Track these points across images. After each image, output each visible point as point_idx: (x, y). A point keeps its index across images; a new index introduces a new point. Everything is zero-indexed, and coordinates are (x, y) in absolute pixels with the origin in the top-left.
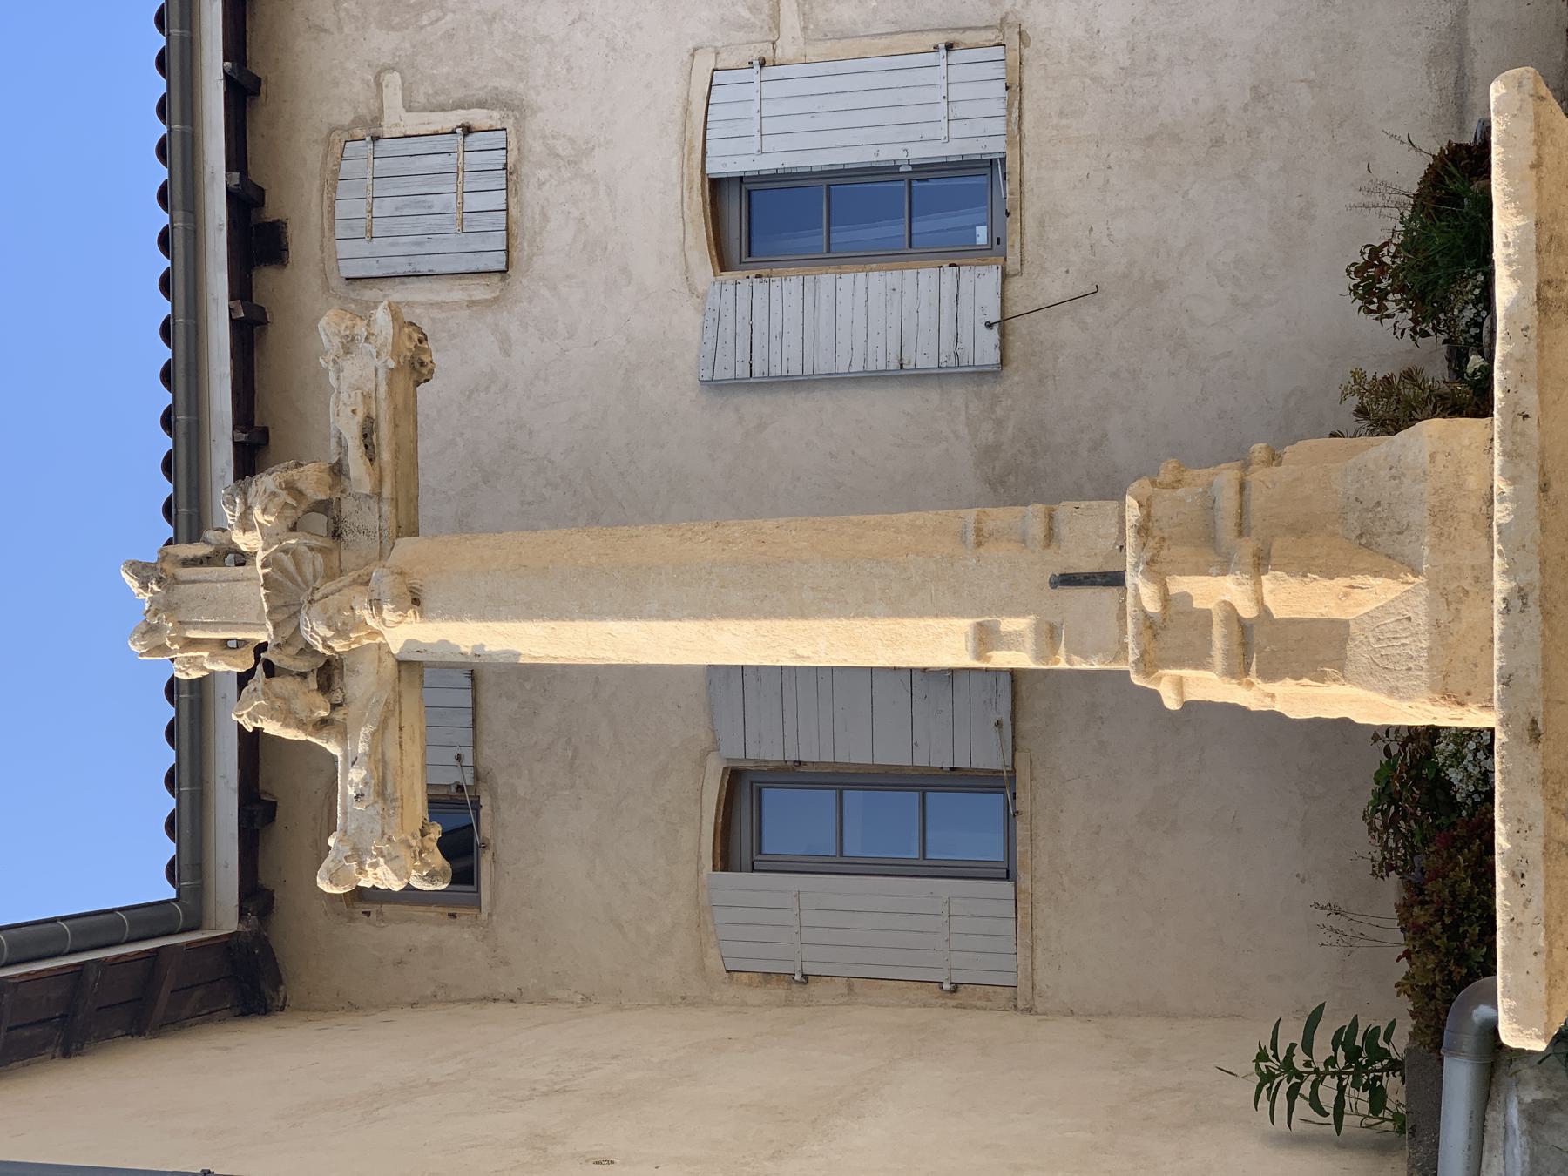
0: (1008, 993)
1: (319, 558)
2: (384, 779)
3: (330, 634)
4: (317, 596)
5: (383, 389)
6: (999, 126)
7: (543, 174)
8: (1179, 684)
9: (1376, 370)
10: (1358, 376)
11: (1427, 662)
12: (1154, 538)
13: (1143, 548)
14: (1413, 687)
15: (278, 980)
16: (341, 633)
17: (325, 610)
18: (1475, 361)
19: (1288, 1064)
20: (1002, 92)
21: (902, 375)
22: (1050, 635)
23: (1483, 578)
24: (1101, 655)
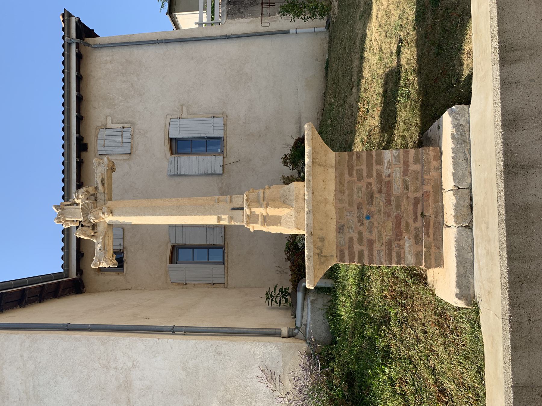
0: (223, 285)
1: (92, 205)
2: (105, 246)
3: (94, 219)
4: (92, 212)
5: (106, 173)
6: (222, 131)
7: (138, 136)
8: (253, 227)
9: (286, 175)
10: (283, 176)
11: (295, 223)
15: (84, 287)
16: (97, 219)
17: (93, 214)
18: (302, 174)
19: (271, 295)
21: (205, 175)
22: (231, 218)
23: (303, 209)
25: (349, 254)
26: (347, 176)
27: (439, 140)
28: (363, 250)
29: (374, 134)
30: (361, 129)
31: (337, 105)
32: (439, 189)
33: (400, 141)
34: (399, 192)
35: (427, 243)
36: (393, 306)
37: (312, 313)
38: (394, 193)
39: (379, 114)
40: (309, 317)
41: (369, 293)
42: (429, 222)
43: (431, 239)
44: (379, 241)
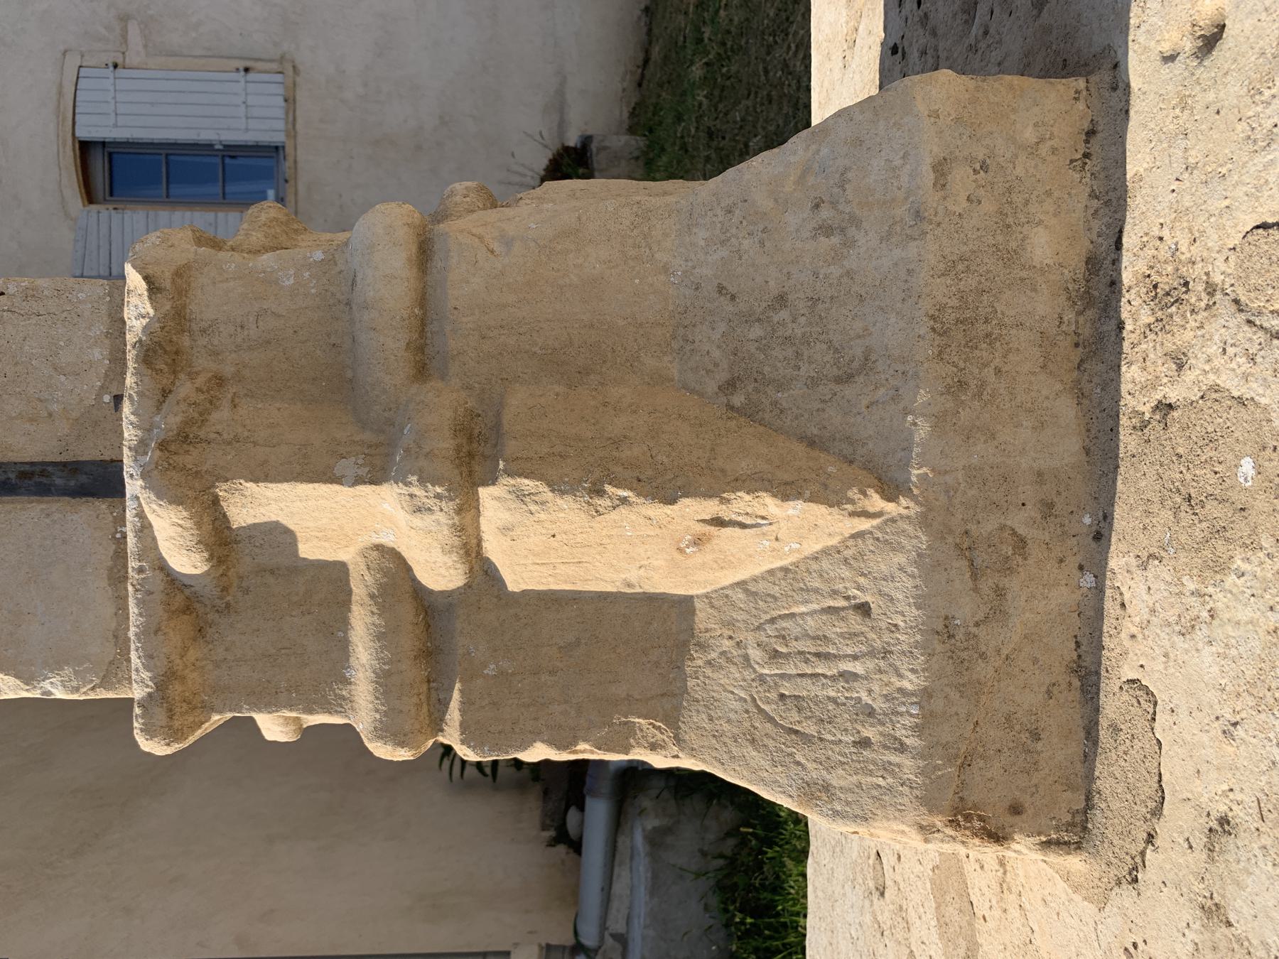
6: (280, 125)
11: (918, 730)
12: (192, 376)
13: (161, 403)
14: (875, 793)
20: (283, 104)
24: (68, 671)
37: (654, 890)
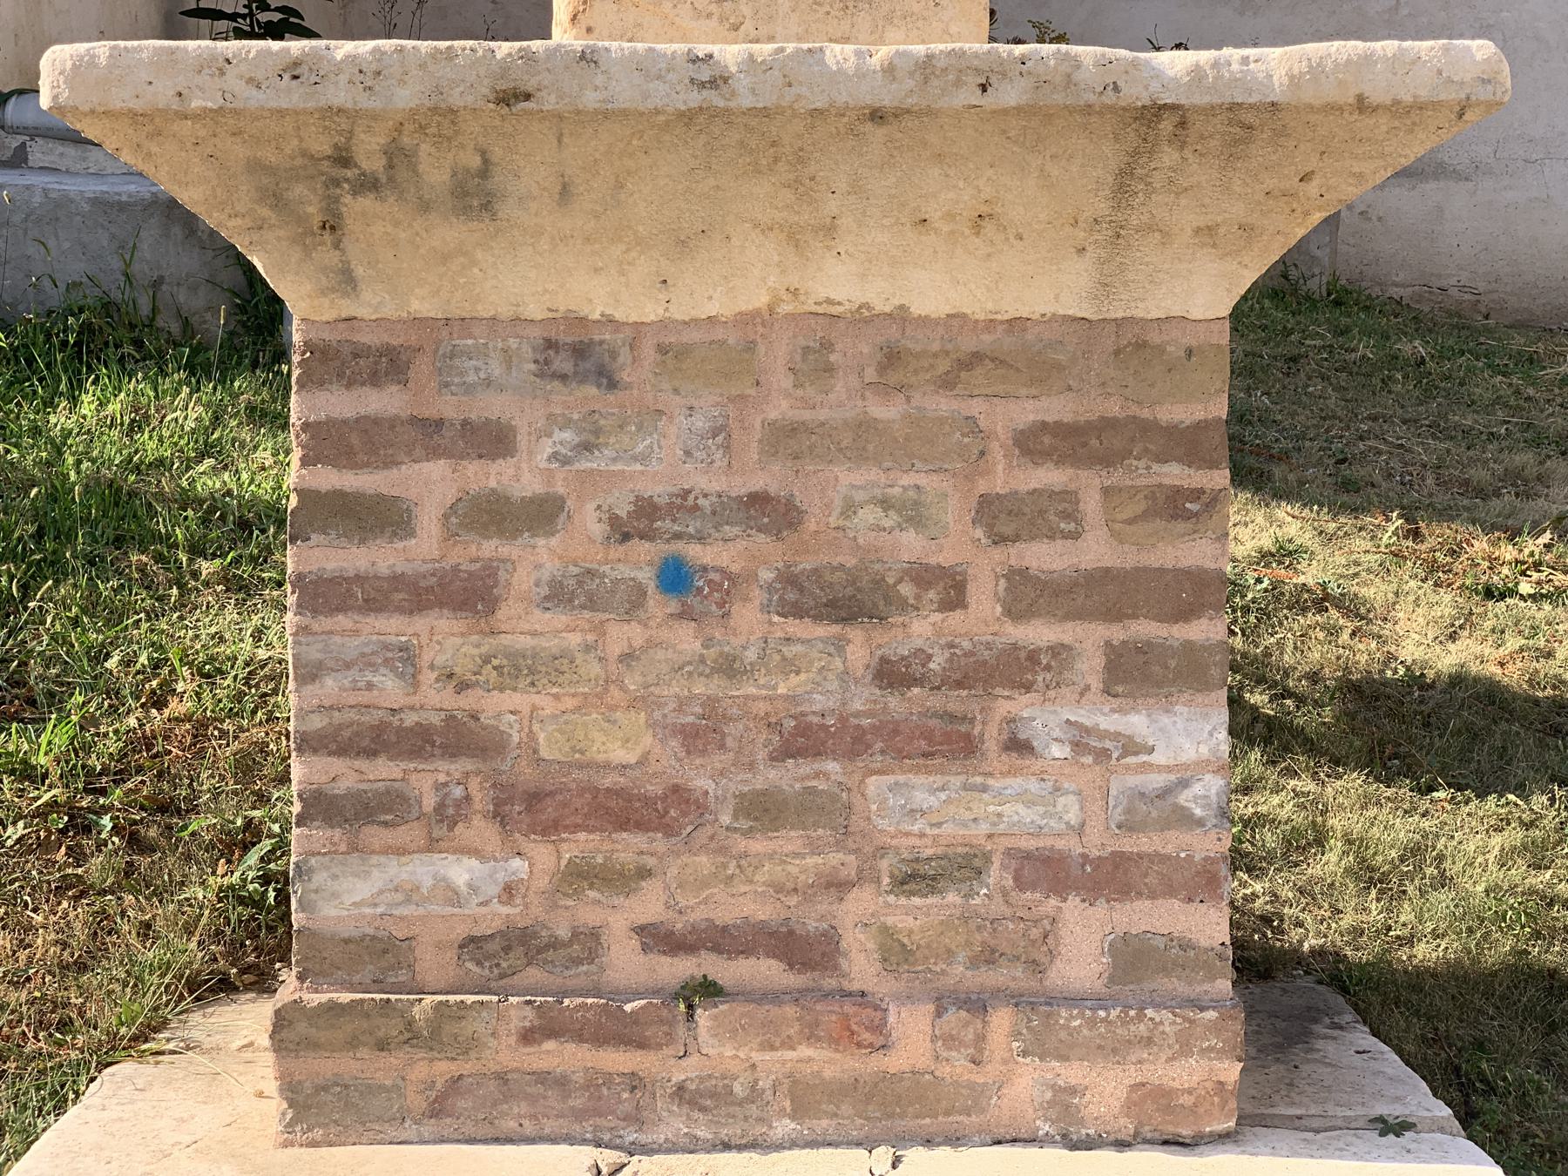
25: (376, 421)
26: (1028, 412)
27: (1295, 1123)
28: (412, 534)
29: (1333, 631)
30: (1369, 545)
31: (1528, 399)
32: (901, 1125)
33: (1283, 814)
34: (882, 824)
35: (476, 1025)
36: (87, 748)
37: (99, 202)
38: (874, 784)
39: (1474, 668)
40: (72, 186)
41: (207, 584)
42: (642, 1045)
43: (505, 1053)
44: (487, 661)
